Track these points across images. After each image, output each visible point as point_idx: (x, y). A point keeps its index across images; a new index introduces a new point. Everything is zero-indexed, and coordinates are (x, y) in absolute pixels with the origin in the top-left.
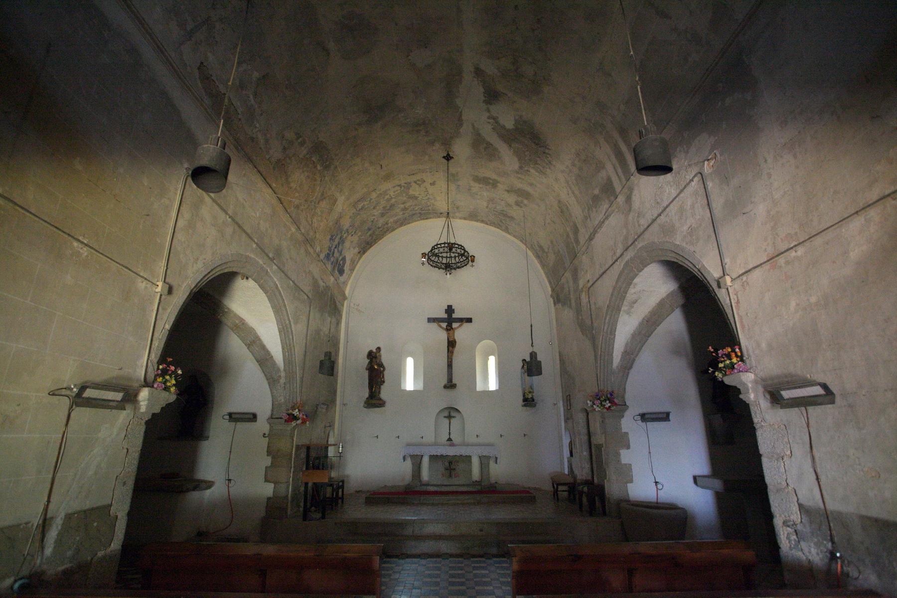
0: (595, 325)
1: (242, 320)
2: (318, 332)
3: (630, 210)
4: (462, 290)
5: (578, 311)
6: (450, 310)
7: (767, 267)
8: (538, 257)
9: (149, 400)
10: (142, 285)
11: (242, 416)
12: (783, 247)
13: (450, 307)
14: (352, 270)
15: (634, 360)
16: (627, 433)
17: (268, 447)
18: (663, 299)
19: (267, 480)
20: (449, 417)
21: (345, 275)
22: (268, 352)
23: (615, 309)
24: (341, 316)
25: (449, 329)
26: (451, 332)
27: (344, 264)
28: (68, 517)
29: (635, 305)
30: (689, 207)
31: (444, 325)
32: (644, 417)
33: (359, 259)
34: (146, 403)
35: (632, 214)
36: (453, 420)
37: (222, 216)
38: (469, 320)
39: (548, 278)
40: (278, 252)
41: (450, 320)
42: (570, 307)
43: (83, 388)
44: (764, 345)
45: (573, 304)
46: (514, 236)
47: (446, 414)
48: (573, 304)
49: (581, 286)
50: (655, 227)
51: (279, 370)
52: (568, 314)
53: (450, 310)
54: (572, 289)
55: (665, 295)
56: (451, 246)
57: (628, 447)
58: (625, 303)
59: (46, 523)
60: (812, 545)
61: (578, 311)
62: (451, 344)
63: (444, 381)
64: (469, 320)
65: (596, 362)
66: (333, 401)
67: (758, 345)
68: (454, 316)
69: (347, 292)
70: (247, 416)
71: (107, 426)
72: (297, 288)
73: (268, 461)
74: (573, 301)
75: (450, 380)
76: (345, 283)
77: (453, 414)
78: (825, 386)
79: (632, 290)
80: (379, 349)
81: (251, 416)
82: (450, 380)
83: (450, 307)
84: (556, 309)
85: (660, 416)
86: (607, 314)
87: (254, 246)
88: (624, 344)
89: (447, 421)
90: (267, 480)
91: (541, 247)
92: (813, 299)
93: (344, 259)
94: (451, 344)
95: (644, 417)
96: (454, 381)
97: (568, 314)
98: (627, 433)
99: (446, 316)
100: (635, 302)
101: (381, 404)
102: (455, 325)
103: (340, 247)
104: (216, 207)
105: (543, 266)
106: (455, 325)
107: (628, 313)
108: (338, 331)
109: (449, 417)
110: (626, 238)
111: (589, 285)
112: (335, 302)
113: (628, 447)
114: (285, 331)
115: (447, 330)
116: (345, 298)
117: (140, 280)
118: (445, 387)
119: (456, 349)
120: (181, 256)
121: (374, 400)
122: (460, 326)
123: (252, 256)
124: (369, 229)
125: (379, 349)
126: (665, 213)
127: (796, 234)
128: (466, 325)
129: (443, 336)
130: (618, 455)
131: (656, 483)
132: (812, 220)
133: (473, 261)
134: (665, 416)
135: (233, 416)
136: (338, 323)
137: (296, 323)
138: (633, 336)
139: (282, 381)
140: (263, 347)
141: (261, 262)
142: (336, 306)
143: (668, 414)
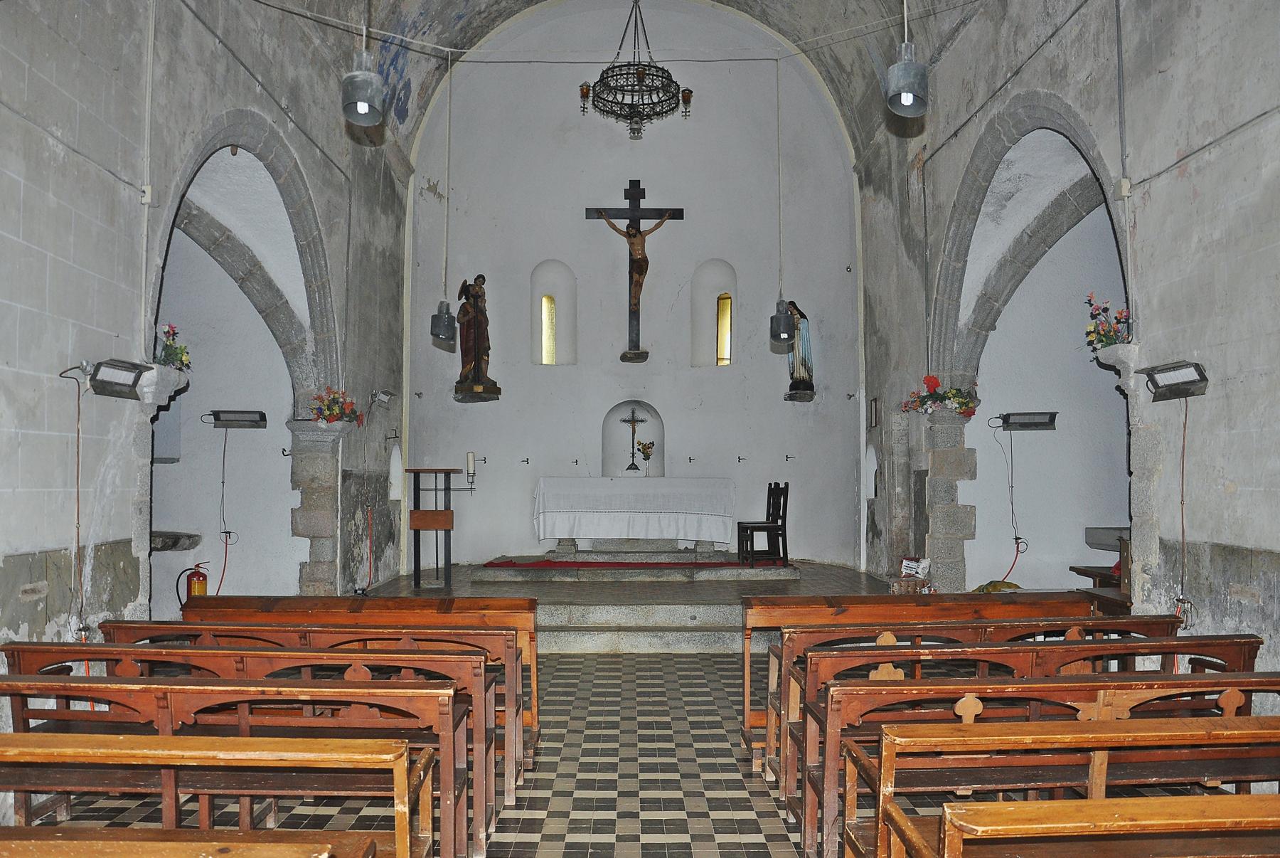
0: (931, 239)
1: (224, 230)
2: (366, 247)
3: (1003, 18)
4: (662, 156)
5: (904, 208)
6: (635, 191)
7: (1175, 172)
8: (830, 80)
9: (157, 384)
10: (125, 192)
11: (238, 417)
12: (1198, 142)
13: (635, 184)
14: (423, 107)
15: (999, 313)
16: (973, 451)
17: (293, 473)
18: (1063, 194)
19: (295, 533)
20: (633, 421)
21: (408, 119)
22: (278, 294)
23: (969, 209)
24: (403, 209)
25: (634, 233)
26: (637, 240)
27: (407, 97)
28: (97, 548)
29: (1010, 204)
30: (1091, 37)
31: (623, 224)
32: (1007, 421)
33: (438, 82)
34: (152, 389)
35: (1006, 25)
36: (639, 427)
37: (211, 43)
38: (677, 214)
39: (849, 126)
40: (295, 92)
41: (634, 213)
42: (890, 196)
43: (97, 367)
44: (1155, 302)
45: (896, 192)
46: (780, 31)
47: (627, 415)
48: (896, 192)
49: (910, 158)
50: (1039, 64)
51: (301, 326)
52: (884, 210)
53: (635, 191)
54: (894, 159)
55: (1068, 186)
56: (641, 72)
57: (973, 476)
58: (989, 198)
59: (81, 551)
60: (1163, 592)
61: (904, 208)
62: (638, 266)
63: (623, 345)
64: (677, 214)
65: (928, 315)
66: (394, 390)
67: (1149, 302)
68: (644, 204)
69: (413, 160)
70: (247, 417)
71: (115, 423)
72: (328, 161)
73: (295, 499)
74: (895, 185)
75: (634, 342)
76: (410, 137)
77: (640, 415)
78: (1198, 367)
79: (1002, 174)
80: (481, 279)
81: (257, 417)
82: (634, 342)
83: (635, 184)
84: (863, 199)
85: (1037, 419)
86: (952, 218)
87: (259, 89)
88: (983, 280)
89: (628, 428)
90: (295, 533)
91: (837, 60)
92: (1217, 235)
93: (407, 86)
94: (638, 266)
95: (1007, 421)
96: (643, 345)
97: (884, 210)
98: (973, 451)
99: (626, 204)
100: (1010, 197)
101: (493, 391)
102: (645, 224)
103: (401, 61)
104: (200, 25)
105: (841, 102)
106: (645, 224)
107: (996, 219)
108: (399, 242)
109: (633, 421)
110: (994, 72)
111: (926, 156)
112: (392, 182)
113: (973, 476)
114: (309, 250)
115: (628, 235)
116: (410, 170)
117: (122, 185)
118: (624, 358)
119: (648, 280)
120: (165, 132)
121: (476, 385)
122: (657, 226)
123: (255, 109)
124: (460, 17)
125: (481, 279)
126: (1056, 39)
127: (1214, 123)
128: (669, 223)
129: (623, 245)
130: (952, 489)
131: (1017, 539)
132: (1232, 106)
133: (687, 101)
134: (1046, 419)
135: (222, 417)
136: (400, 225)
137: (329, 234)
138: (1002, 266)
139: (310, 348)
140: (269, 284)
141: (269, 120)
142: (393, 189)
143: (1053, 416)
